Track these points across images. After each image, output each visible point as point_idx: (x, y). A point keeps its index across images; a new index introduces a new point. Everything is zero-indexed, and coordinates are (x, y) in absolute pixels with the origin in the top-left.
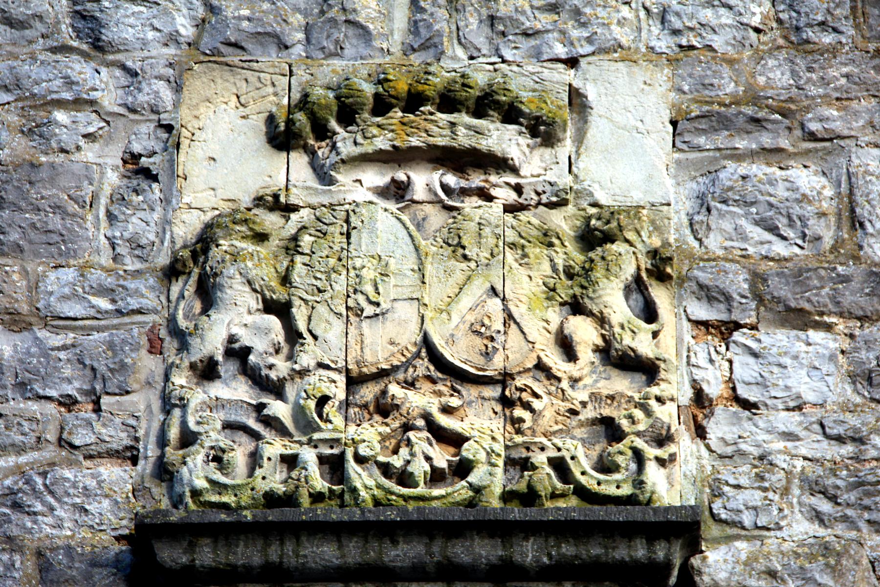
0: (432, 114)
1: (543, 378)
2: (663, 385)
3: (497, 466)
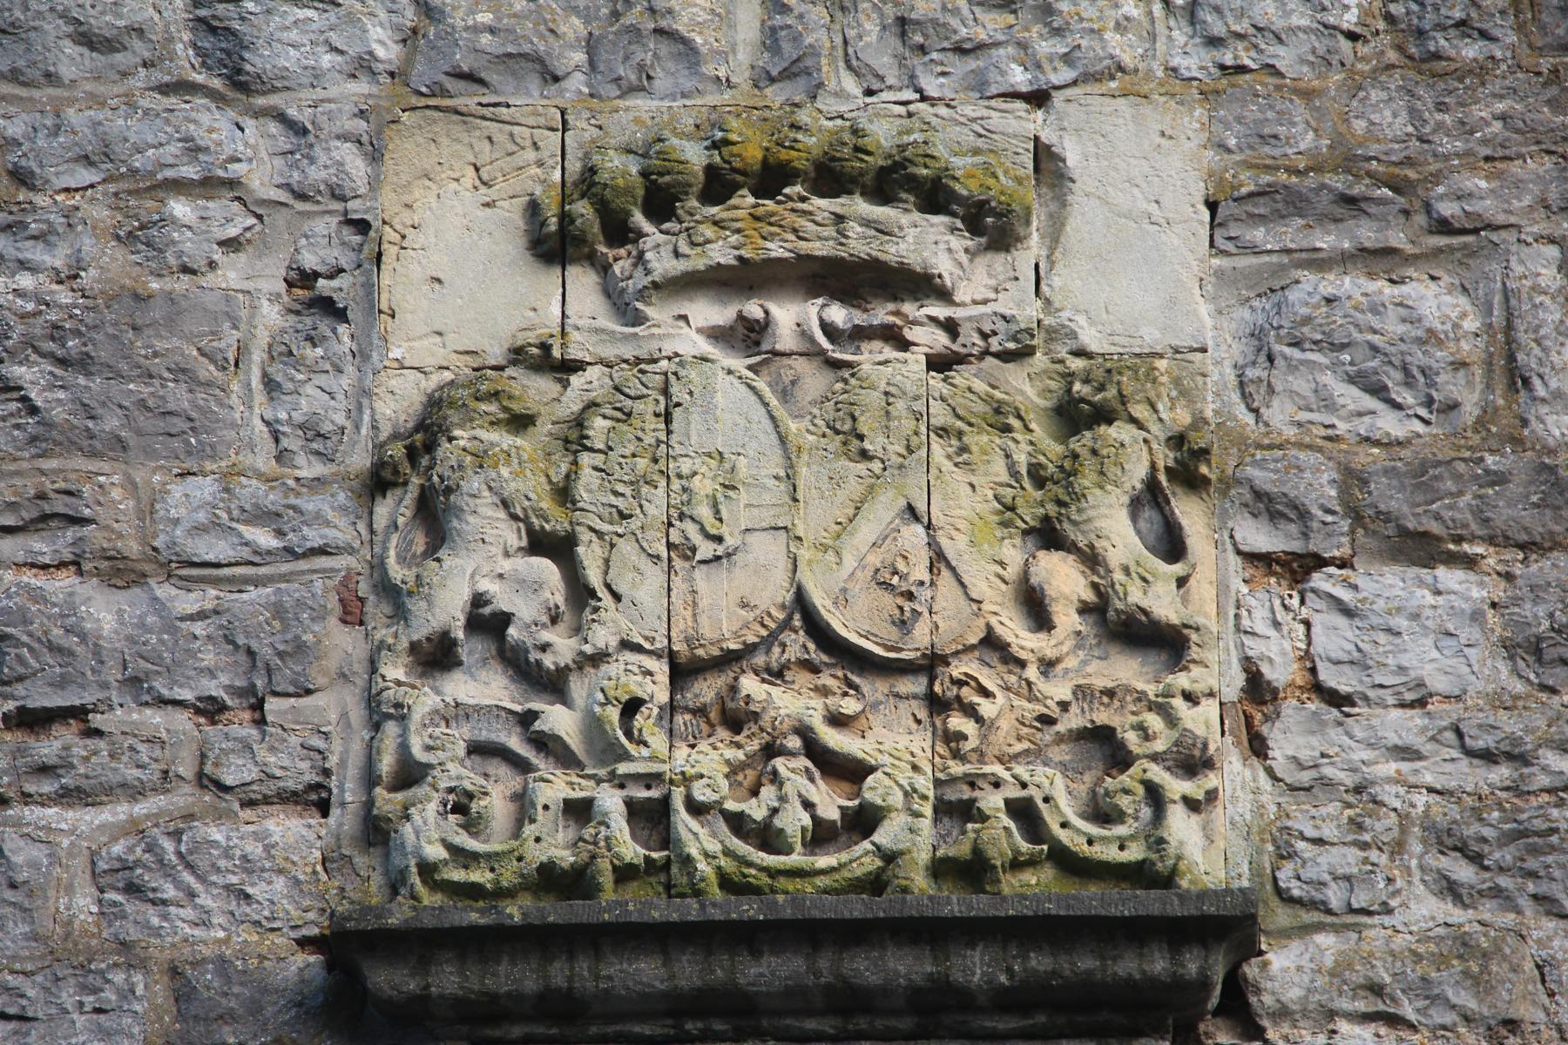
0: (803, 199)
1: (995, 661)
2: (1196, 671)
3: (922, 816)
